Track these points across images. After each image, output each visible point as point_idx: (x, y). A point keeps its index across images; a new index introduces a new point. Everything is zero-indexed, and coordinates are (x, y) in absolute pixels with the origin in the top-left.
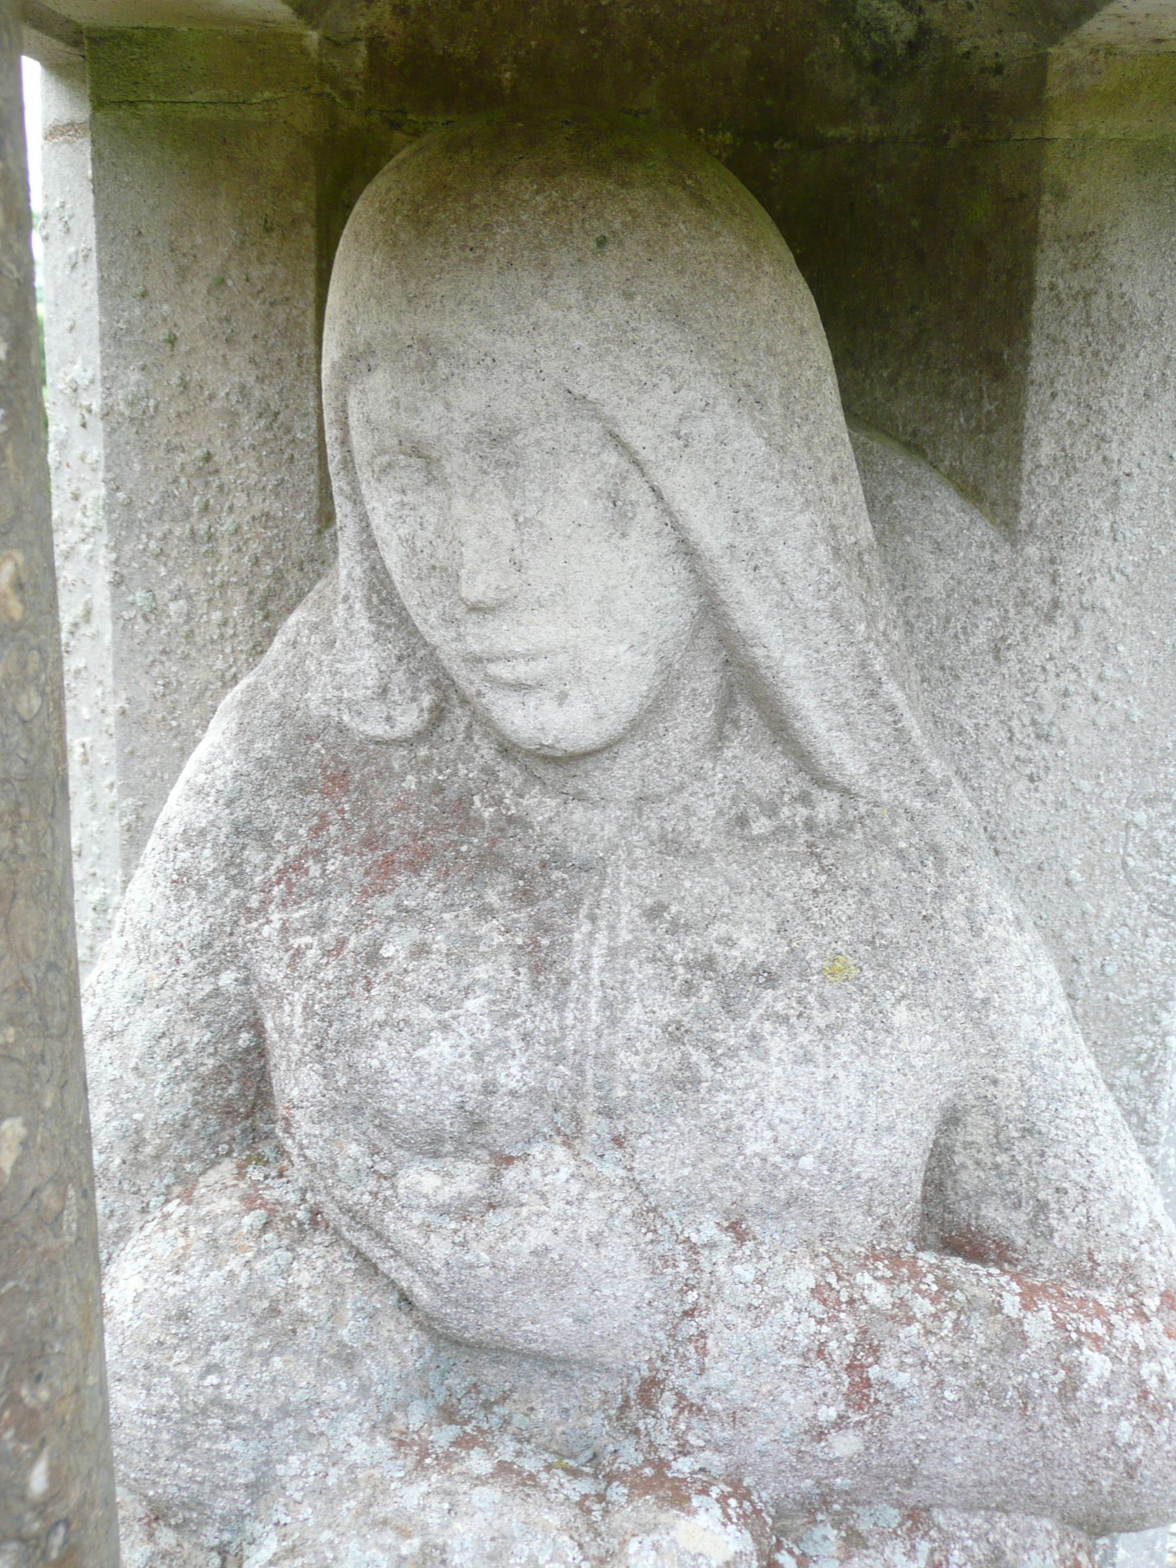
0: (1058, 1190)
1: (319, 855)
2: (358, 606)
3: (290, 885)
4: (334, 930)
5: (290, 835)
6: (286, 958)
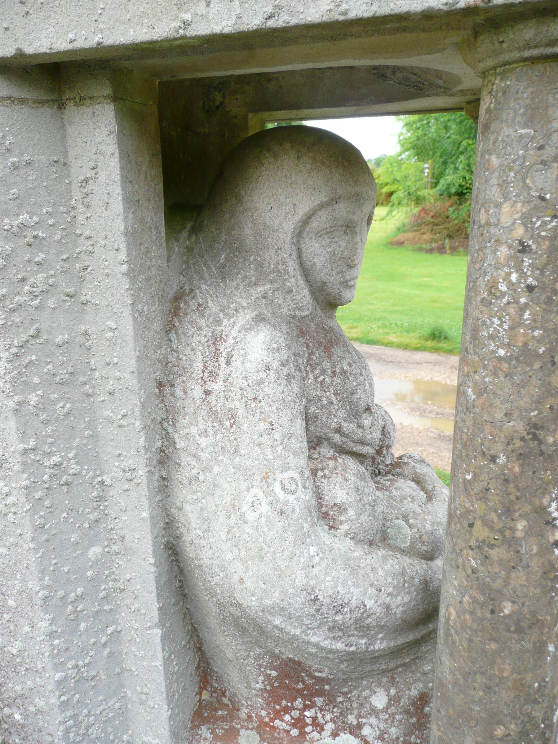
0: (206, 431)
1: (312, 353)
2: (299, 277)
3: (311, 365)
4: (329, 370)
5: (304, 351)
6: (319, 386)
